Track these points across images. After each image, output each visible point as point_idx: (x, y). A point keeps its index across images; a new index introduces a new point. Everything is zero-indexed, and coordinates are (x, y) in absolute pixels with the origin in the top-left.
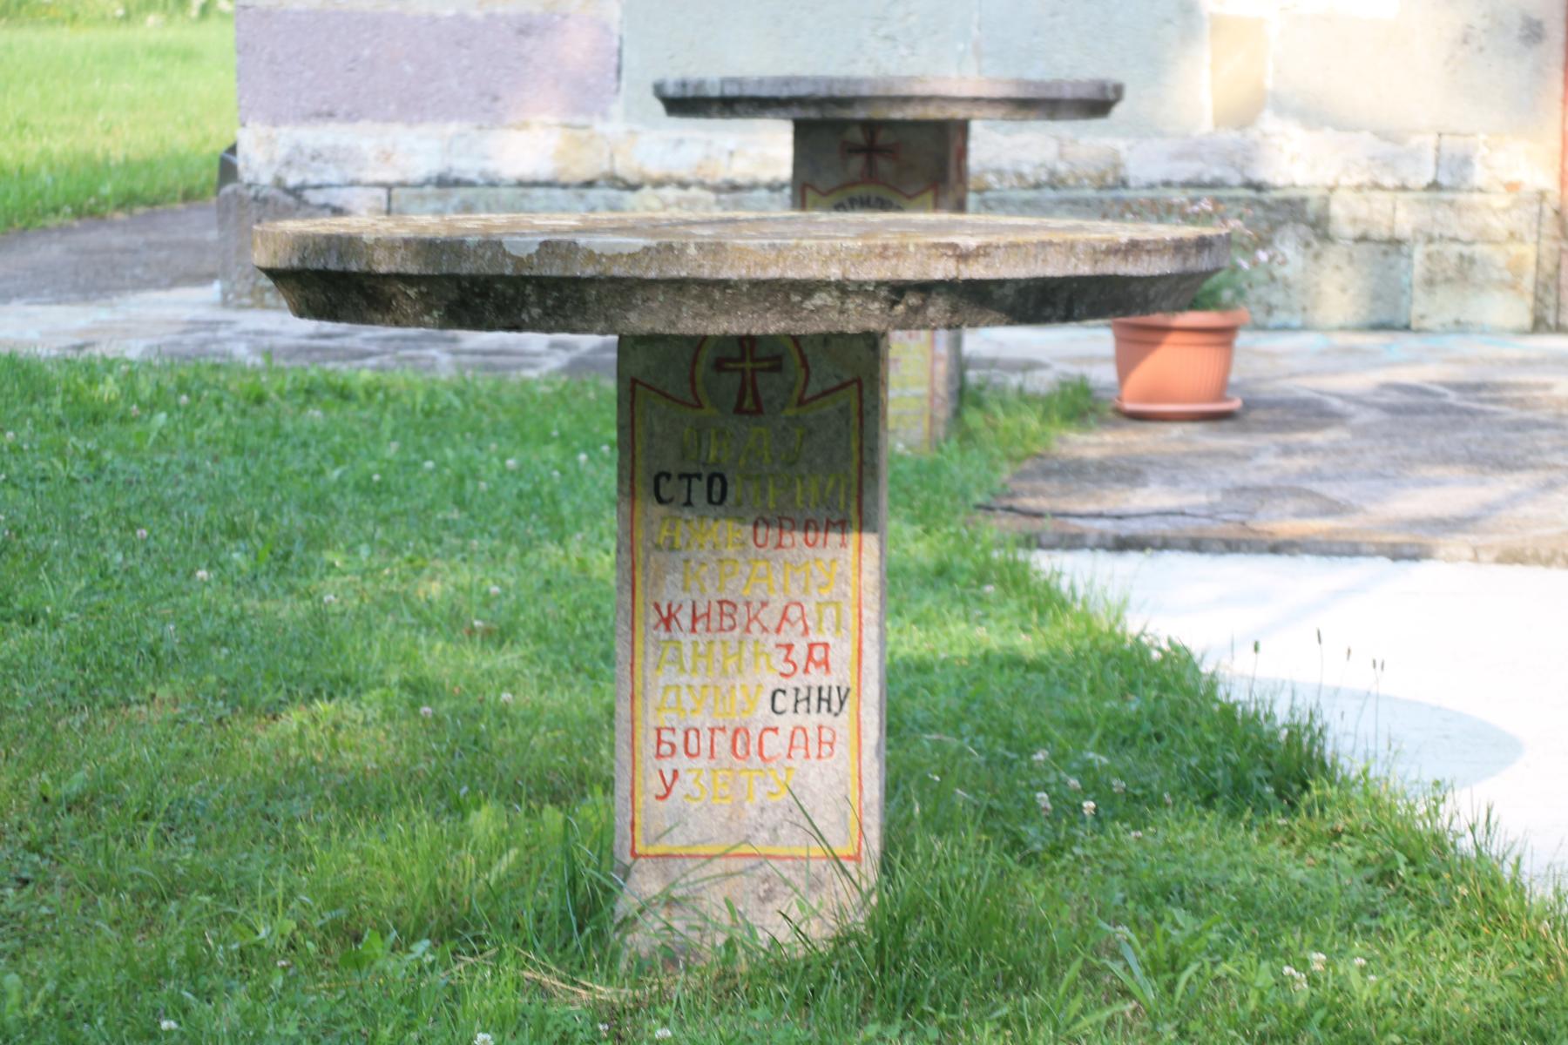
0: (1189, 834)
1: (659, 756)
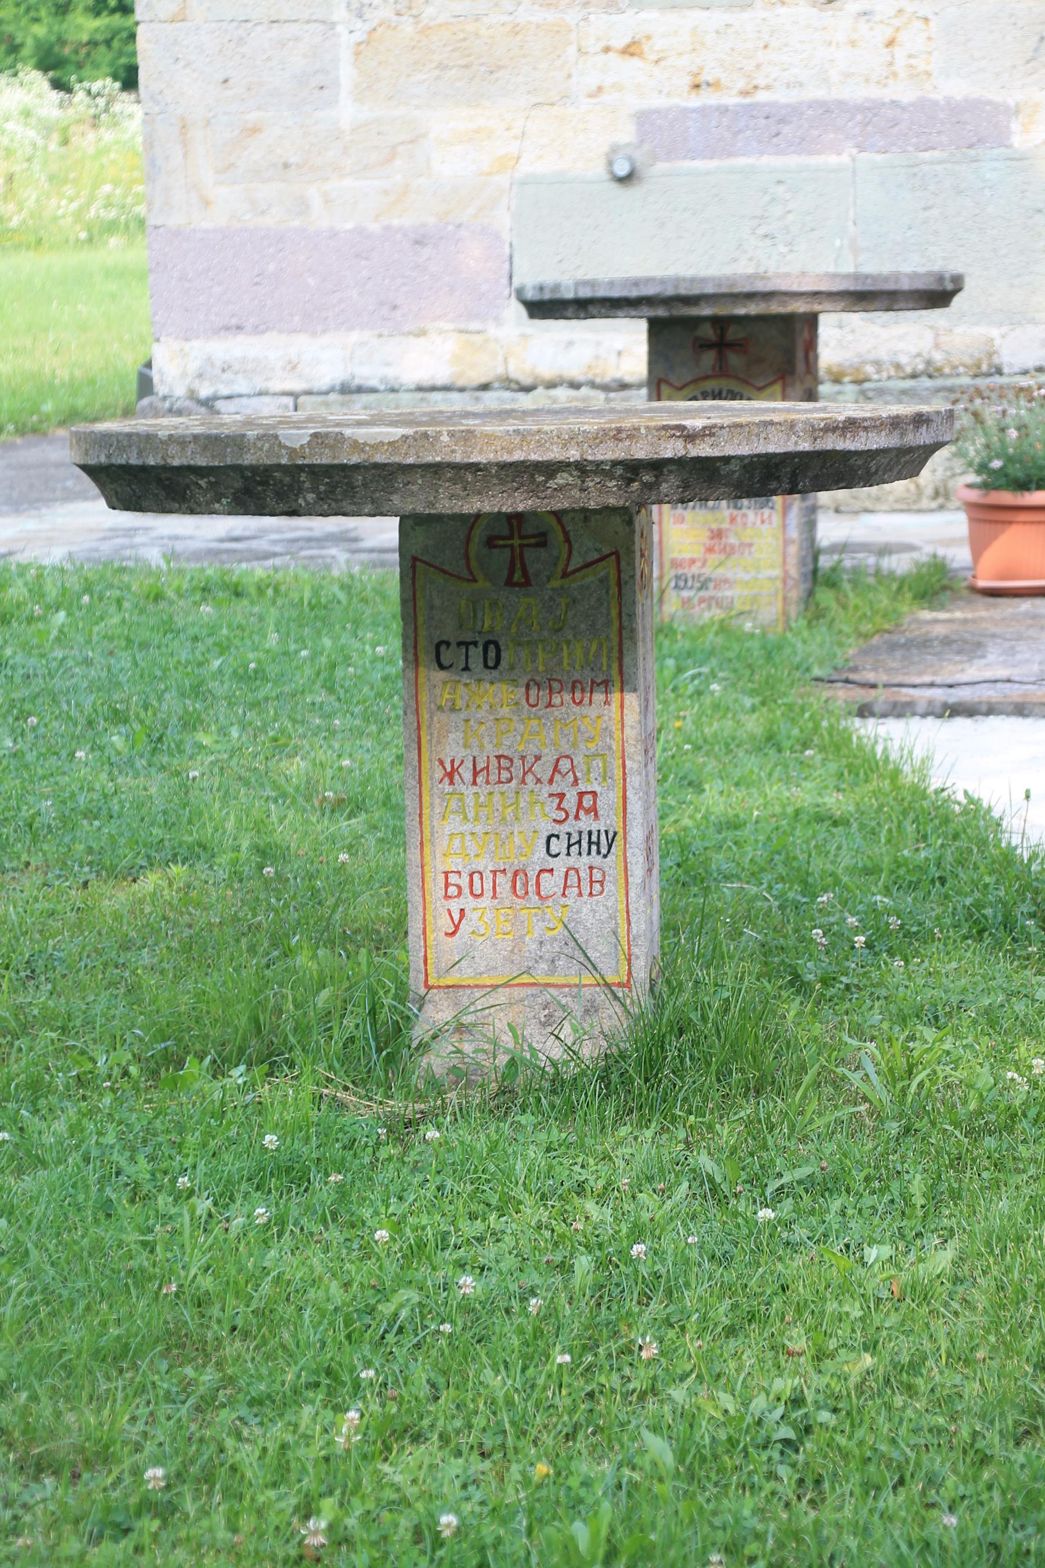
0: (954, 965)
1: (447, 897)
